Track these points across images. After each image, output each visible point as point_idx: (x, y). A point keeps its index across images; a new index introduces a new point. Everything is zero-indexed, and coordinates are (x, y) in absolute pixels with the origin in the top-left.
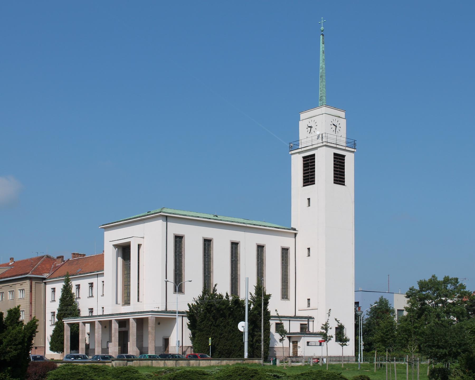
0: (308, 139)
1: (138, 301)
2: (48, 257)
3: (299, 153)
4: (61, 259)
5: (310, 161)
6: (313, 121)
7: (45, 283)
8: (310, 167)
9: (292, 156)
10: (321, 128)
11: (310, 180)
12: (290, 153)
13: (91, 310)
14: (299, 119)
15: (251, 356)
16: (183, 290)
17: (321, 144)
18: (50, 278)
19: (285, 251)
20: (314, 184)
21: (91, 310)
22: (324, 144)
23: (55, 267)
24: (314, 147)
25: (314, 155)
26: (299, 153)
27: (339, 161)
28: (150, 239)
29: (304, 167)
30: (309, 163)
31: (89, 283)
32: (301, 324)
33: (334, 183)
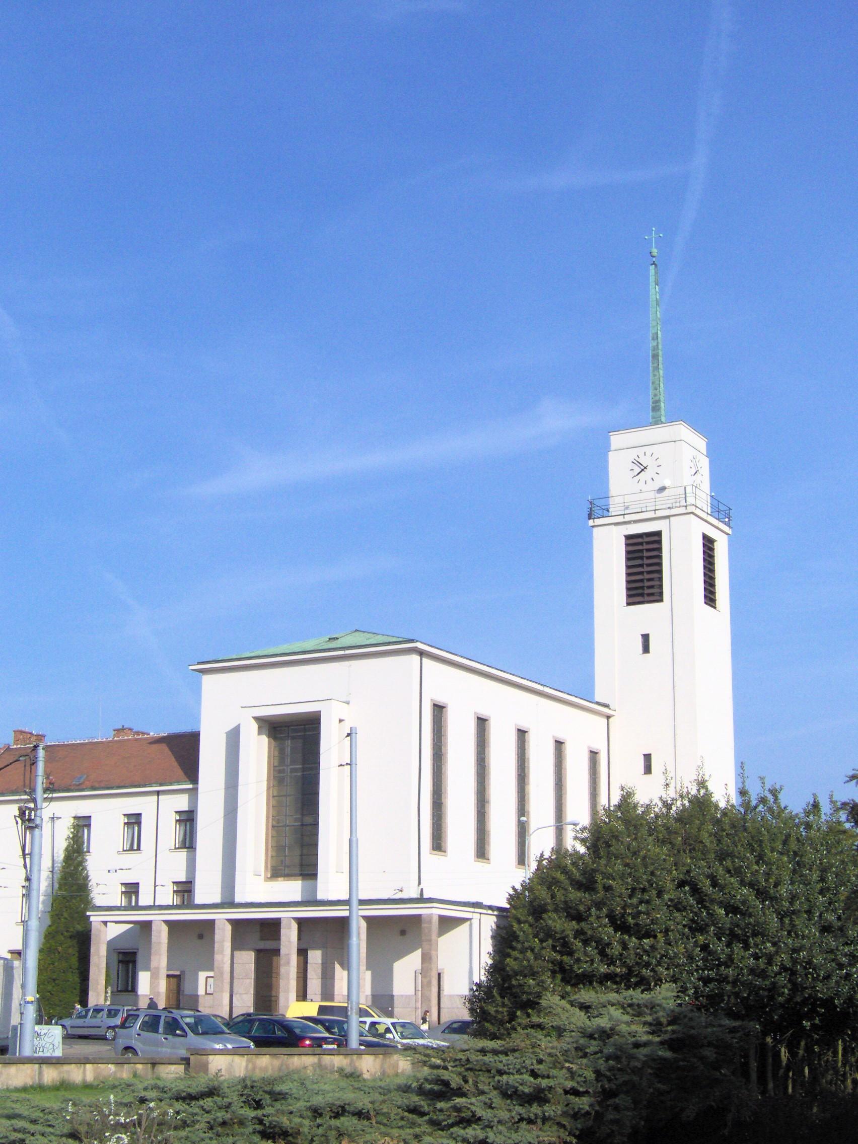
5: (646, 547)
8: (646, 561)
9: (595, 530)
11: (647, 591)
12: (591, 522)
13: (132, 889)
14: (607, 448)
17: (683, 510)
20: (661, 600)
21: (132, 889)
22: (690, 509)
25: (659, 534)
28: (370, 712)
31: (127, 815)
32: (628, 537)
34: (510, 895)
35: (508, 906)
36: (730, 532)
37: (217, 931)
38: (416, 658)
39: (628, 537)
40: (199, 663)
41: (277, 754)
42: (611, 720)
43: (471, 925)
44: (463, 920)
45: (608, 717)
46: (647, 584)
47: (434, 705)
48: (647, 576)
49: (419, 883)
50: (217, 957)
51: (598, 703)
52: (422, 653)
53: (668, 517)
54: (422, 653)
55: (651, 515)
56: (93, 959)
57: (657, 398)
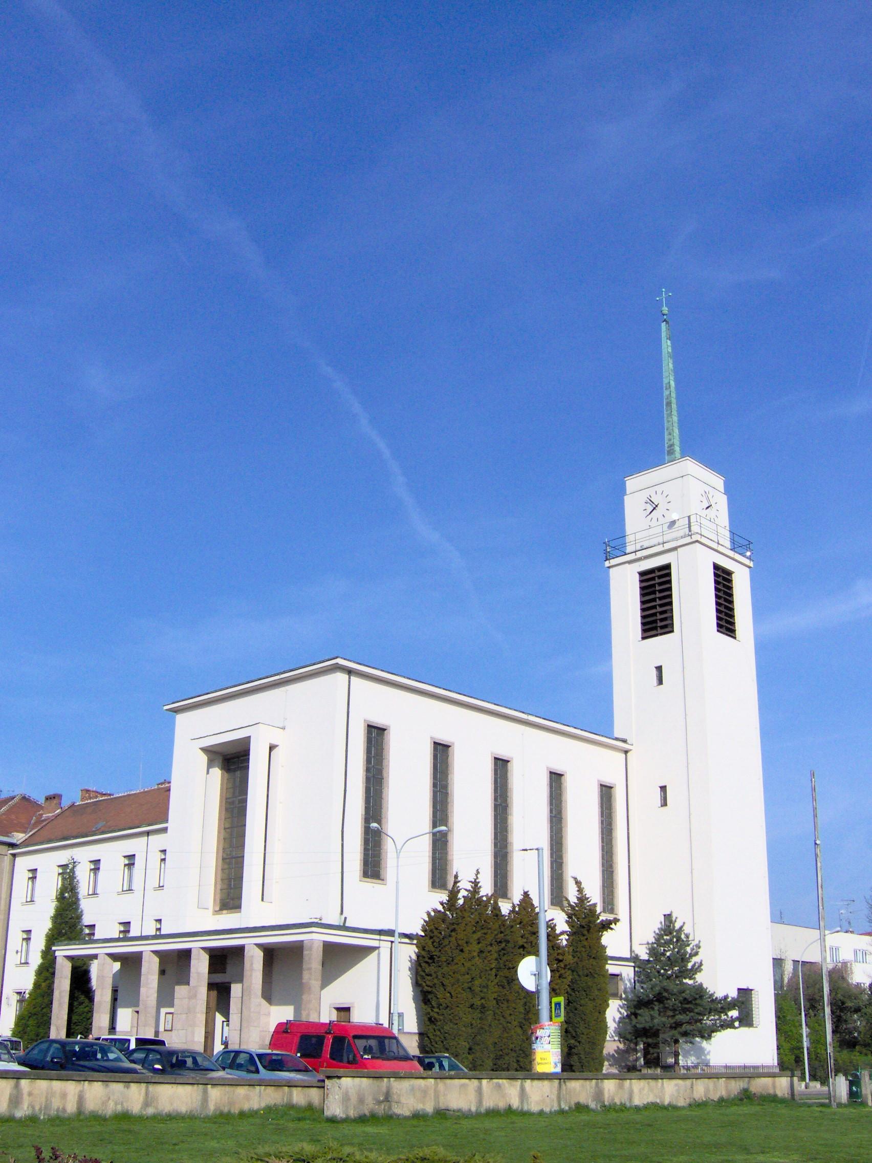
0: (652, 531)
1: (263, 900)
2: (24, 798)
3: (630, 562)
4: (55, 801)
5: (657, 581)
7: (14, 855)
8: (658, 595)
10: (680, 507)
11: (660, 624)
12: (607, 564)
15: (578, 1058)
16: (382, 872)
17: (688, 540)
18: (25, 843)
20: (672, 631)
22: (695, 538)
23: (39, 821)
24: (667, 546)
25: (668, 567)
26: (630, 562)
32: (642, 574)
34: (425, 921)
35: (423, 934)
36: (751, 564)
38: (342, 677)
39: (642, 574)
41: (230, 785)
42: (629, 754)
43: (379, 954)
44: (371, 949)
45: (626, 752)
46: (659, 617)
47: (435, 743)
48: (659, 609)
49: (342, 913)
50: (143, 990)
51: (617, 739)
52: (350, 672)
53: (675, 549)
54: (350, 672)
56: (56, 994)
57: (671, 443)
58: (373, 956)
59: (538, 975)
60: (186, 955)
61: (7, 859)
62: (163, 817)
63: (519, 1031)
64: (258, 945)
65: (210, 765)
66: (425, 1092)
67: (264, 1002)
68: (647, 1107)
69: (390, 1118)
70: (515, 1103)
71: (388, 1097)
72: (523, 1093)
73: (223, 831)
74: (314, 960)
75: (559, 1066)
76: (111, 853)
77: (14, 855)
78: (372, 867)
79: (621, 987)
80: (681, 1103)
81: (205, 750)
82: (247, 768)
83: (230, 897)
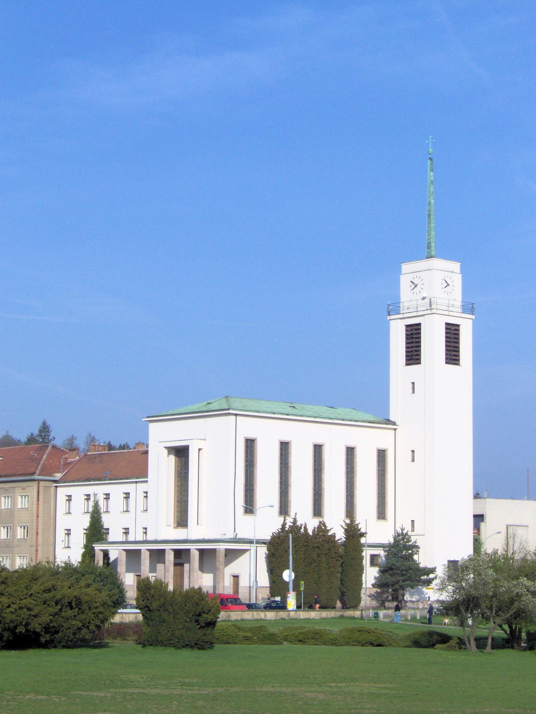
4: (75, 452)
6: (418, 277)
9: (391, 321)
12: (388, 318)
13: (126, 532)
17: (429, 312)
19: (382, 455)
20: (420, 363)
21: (126, 532)
24: (419, 313)
25: (419, 325)
27: (452, 333)
29: (407, 339)
30: (413, 335)
32: (407, 326)
33: (446, 363)
37: (142, 555)
40: (148, 417)
44: (245, 551)
49: (235, 531)
50: (142, 567)
55: (415, 314)
58: (247, 554)
59: (290, 576)
60: (162, 552)
61: (53, 489)
62: (146, 476)
63: (316, 586)
64: (197, 549)
65: (169, 454)
66: (238, 615)
67: (200, 572)
68: (304, 619)
69: (230, 621)
70: (263, 617)
71: (229, 616)
72: (265, 615)
73: (177, 487)
74: (221, 557)
75: (295, 607)
76: (116, 490)
77: (56, 487)
78: (249, 508)
79: (380, 560)
80: (317, 618)
81: (166, 448)
82: (188, 456)
83: (182, 520)
